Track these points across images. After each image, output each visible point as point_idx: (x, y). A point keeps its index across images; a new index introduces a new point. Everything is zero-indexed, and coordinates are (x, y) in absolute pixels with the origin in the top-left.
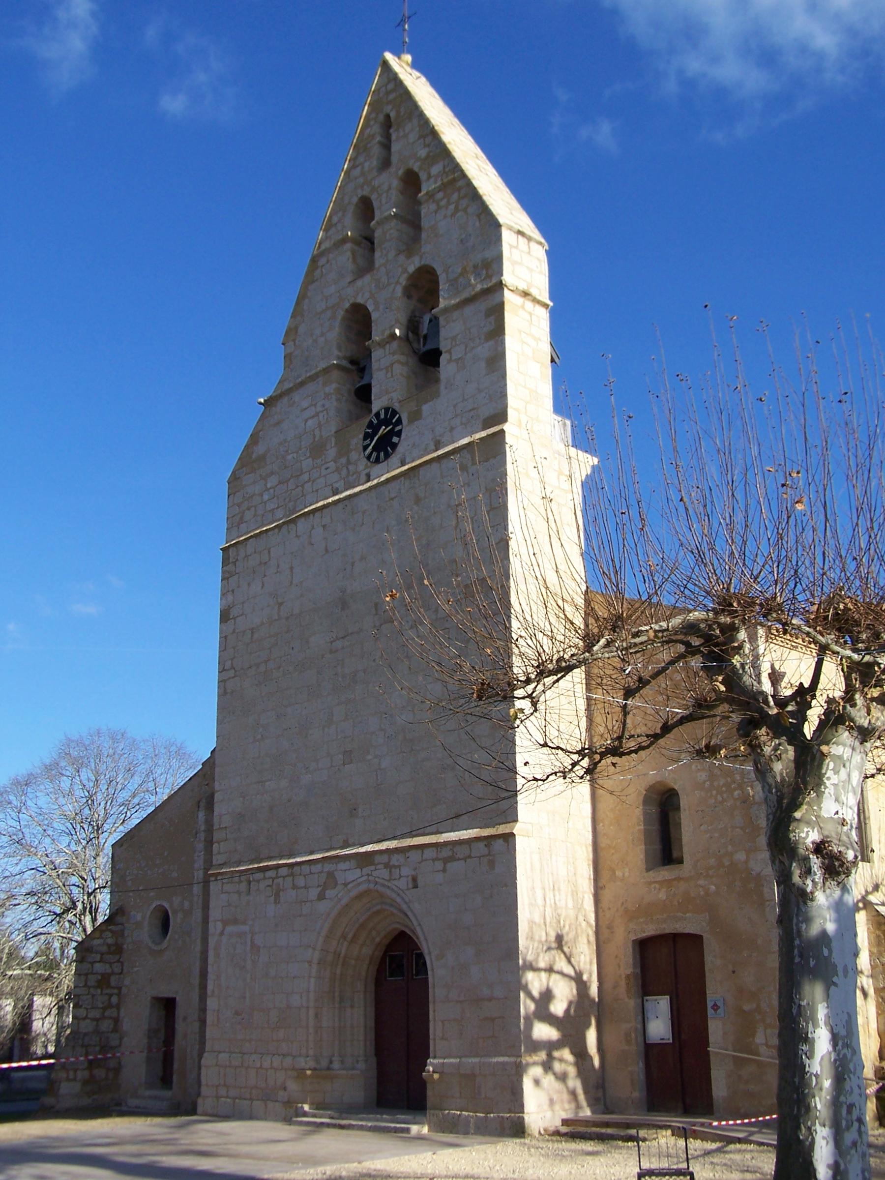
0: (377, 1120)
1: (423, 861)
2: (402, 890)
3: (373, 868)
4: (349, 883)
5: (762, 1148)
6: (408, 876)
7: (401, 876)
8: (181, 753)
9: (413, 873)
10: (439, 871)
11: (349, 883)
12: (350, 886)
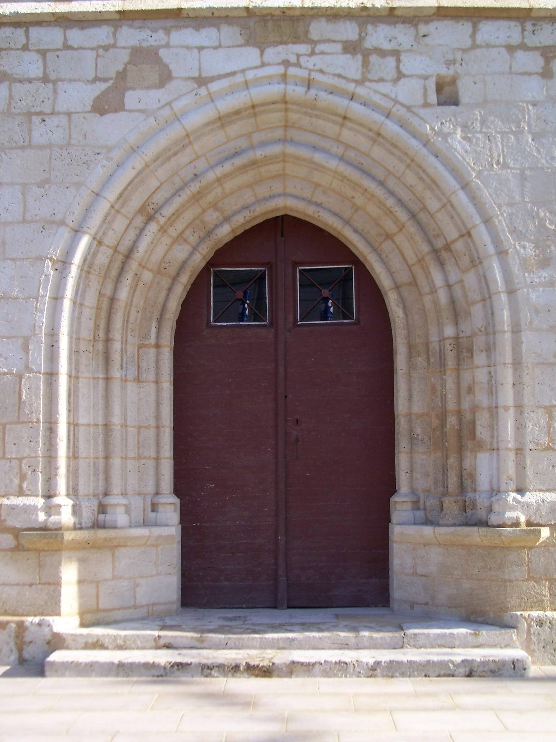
0: (345, 646)
1: (475, 46)
2: (409, 108)
3: (303, 48)
4: (213, 79)
5: (140, 373)
6: (426, 78)
7: (400, 75)
8: (283, 48)
9: (443, 71)
10: (529, 74)
11: (213, 79)
12: (214, 87)
